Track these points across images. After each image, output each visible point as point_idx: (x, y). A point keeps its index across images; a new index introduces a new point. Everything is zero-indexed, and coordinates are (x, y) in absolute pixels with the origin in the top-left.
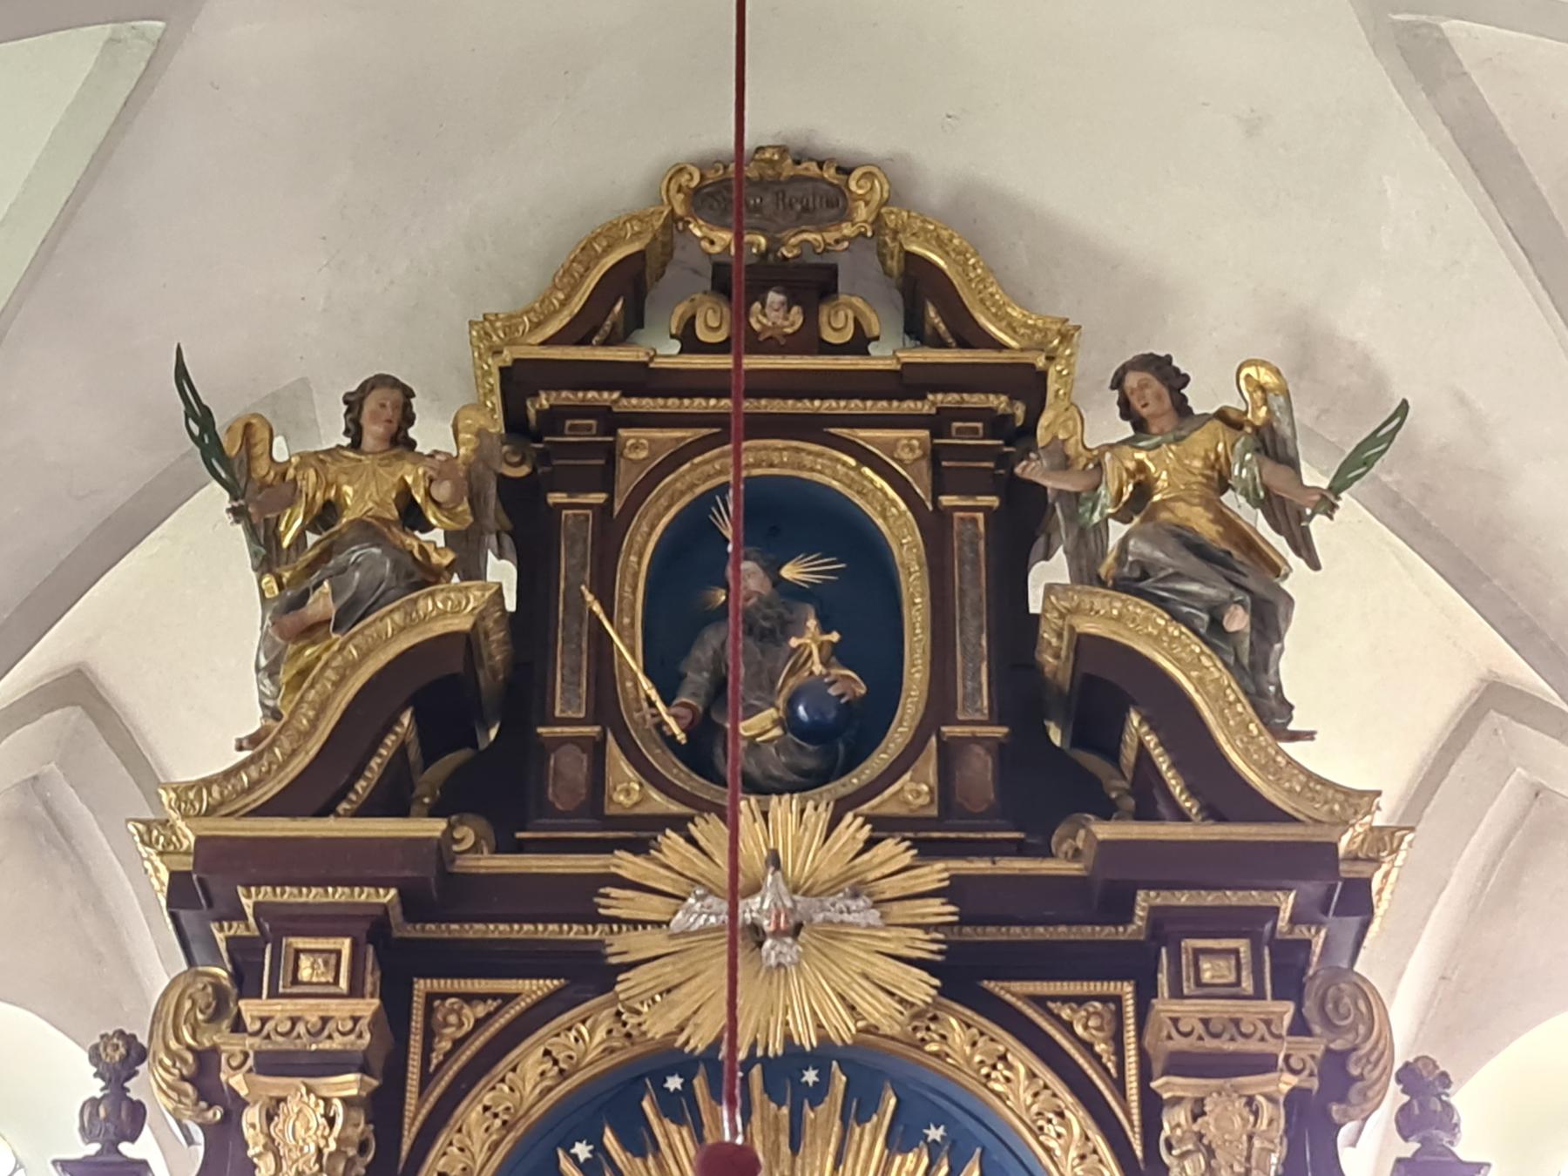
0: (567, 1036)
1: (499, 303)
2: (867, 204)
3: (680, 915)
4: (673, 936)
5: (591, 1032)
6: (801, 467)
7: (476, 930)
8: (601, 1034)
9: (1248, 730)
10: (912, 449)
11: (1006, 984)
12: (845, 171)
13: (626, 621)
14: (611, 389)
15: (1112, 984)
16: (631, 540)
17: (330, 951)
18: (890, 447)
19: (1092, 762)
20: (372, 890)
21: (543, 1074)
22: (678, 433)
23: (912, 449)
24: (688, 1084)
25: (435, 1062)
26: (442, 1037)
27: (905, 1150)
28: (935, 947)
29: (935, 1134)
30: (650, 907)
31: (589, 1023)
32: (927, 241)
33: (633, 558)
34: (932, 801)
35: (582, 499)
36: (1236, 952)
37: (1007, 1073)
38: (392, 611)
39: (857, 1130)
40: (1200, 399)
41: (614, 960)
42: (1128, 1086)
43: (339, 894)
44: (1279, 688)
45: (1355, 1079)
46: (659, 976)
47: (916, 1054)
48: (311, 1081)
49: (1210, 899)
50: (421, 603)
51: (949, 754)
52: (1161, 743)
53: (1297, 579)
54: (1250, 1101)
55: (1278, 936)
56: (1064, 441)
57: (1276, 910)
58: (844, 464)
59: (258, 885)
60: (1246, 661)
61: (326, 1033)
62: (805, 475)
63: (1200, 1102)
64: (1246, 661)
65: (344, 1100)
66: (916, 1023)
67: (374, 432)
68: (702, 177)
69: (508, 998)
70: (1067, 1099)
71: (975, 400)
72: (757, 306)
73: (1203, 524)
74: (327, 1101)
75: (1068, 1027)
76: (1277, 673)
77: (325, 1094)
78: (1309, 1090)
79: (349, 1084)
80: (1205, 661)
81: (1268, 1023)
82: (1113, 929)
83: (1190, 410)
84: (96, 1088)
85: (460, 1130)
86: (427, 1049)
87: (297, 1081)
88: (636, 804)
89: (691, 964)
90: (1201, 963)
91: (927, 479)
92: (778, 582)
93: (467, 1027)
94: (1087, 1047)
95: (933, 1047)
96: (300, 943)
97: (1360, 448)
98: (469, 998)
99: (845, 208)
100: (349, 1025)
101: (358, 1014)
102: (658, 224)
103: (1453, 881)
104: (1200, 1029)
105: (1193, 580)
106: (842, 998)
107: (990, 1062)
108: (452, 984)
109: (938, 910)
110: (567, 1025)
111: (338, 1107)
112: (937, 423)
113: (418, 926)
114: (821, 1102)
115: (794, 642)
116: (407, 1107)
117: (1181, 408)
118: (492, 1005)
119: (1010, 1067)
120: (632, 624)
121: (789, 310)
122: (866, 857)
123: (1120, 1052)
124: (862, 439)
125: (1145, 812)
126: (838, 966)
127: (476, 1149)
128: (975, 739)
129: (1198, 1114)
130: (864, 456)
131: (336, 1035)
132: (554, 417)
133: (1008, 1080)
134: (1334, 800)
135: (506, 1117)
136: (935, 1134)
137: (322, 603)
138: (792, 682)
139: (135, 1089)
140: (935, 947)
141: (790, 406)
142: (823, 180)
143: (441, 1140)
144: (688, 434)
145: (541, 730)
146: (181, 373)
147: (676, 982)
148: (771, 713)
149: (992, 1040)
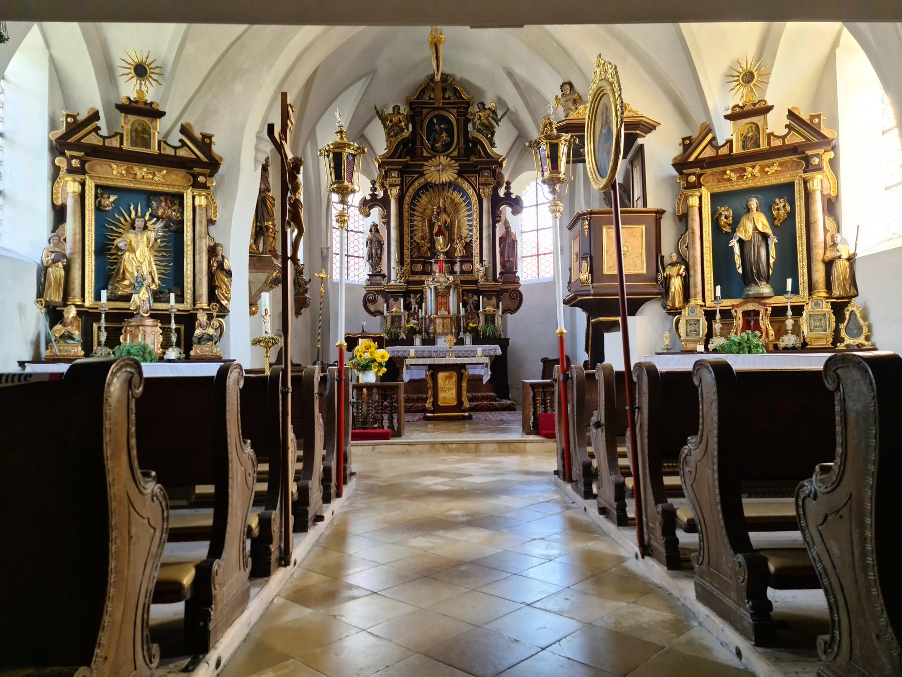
19: (474, 149)
30: (428, 168)
40: (487, 107)
53: (497, 129)
67: (396, 112)
71: (462, 105)
73: (485, 121)
79: (398, 187)
109: (457, 168)
112: (458, 108)
117: (485, 108)
125: (480, 158)
130: (450, 112)
137: (392, 134)
139: (375, 186)
146: (375, 107)
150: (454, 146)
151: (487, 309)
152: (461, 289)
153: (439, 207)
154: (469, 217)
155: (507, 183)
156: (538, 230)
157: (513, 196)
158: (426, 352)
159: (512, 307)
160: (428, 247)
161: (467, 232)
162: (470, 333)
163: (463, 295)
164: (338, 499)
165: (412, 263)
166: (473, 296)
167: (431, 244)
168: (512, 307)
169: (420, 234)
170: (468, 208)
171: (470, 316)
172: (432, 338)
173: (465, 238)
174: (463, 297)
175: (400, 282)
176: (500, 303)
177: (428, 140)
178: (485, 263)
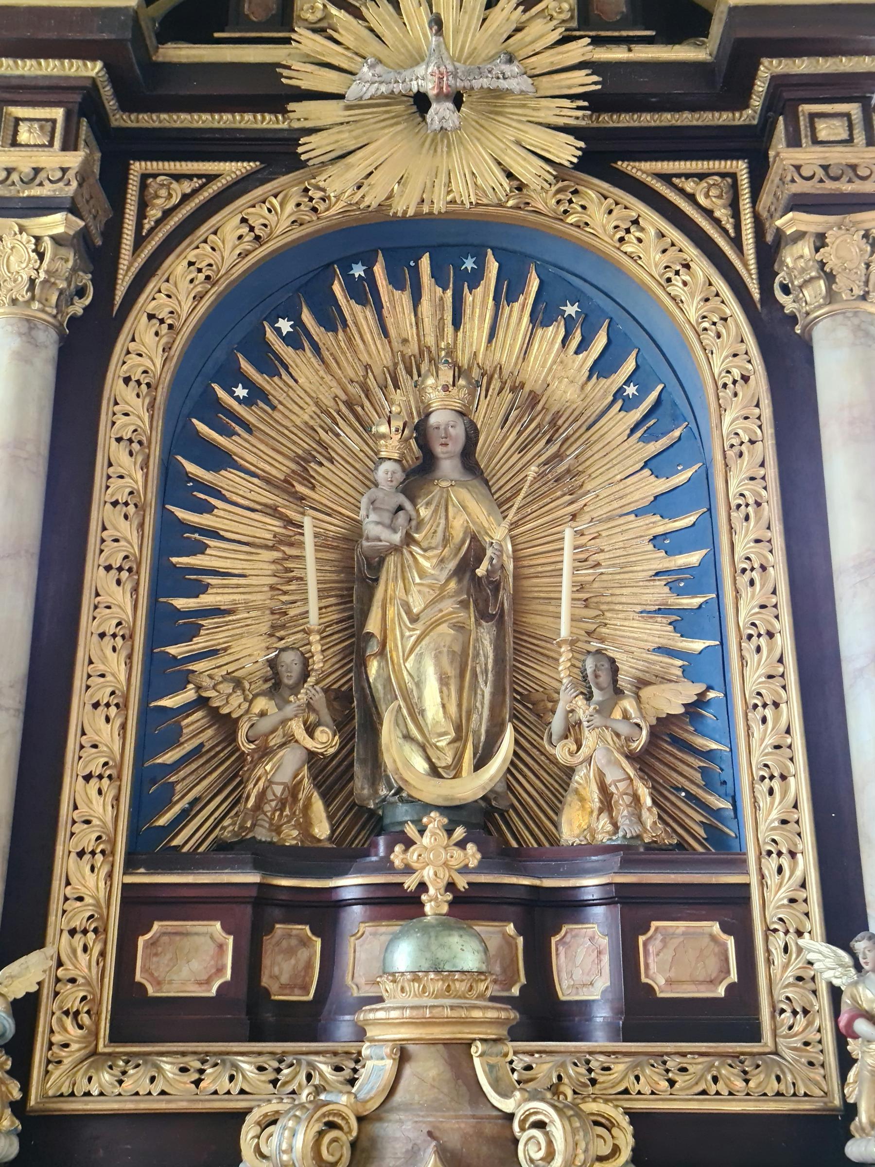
0: (261, 207)
3: (354, 86)
4: (348, 108)
5: (282, 204)
11: (637, 164)
15: (729, 162)
17: (47, 120)
20: (80, 62)
21: (240, 237)
24: (369, 272)
25: (147, 227)
26: (153, 206)
27: (546, 324)
28: (580, 113)
29: (571, 310)
31: (280, 197)
34: (572, 17)
36: (848, 115)
37: (638, 234)
39: (507, 310)
42: (745, 243)
46: (337, 141)
47: (558, 225)
48: (23, 222)
61: (37, 181)
65: (53, 238)
66: (559, 196)
69: (211, 178)
70: (692, 252)
74: (38, 239)
75: (691, 198)
77: (37, 232)
82: (730, 115)
85: (167, 281)
86: (141, 215)
88: (320, 20)
89: (365, 133)
90: (817, 125)
93: (175, 200)
94: (708, 213)
95: (571, 219)
98: (178, 177)
100: (59, 174)
101: (65, 166)
104: (820, 173)
107: (624, 226)
108: (163, 165)
110: (261, 198)
111: (47, 245)
113: (133, 117)
114: (476, 287)
116: (121, 261)
118: (196, 183)
119: (642, 230)
122: (519, 36)
123: (736, 215)
126: (494, 135)
129: (820, 241)
131: (46, 183)
133: (640, 240)
135: (209, 273)
136: (571, 310)
143: (151, 286)
147: (353, 148)
149: (626, 208)
167: (341, 725)
170: (654, 448)
173: (641, 683)
174: (481, 1040)
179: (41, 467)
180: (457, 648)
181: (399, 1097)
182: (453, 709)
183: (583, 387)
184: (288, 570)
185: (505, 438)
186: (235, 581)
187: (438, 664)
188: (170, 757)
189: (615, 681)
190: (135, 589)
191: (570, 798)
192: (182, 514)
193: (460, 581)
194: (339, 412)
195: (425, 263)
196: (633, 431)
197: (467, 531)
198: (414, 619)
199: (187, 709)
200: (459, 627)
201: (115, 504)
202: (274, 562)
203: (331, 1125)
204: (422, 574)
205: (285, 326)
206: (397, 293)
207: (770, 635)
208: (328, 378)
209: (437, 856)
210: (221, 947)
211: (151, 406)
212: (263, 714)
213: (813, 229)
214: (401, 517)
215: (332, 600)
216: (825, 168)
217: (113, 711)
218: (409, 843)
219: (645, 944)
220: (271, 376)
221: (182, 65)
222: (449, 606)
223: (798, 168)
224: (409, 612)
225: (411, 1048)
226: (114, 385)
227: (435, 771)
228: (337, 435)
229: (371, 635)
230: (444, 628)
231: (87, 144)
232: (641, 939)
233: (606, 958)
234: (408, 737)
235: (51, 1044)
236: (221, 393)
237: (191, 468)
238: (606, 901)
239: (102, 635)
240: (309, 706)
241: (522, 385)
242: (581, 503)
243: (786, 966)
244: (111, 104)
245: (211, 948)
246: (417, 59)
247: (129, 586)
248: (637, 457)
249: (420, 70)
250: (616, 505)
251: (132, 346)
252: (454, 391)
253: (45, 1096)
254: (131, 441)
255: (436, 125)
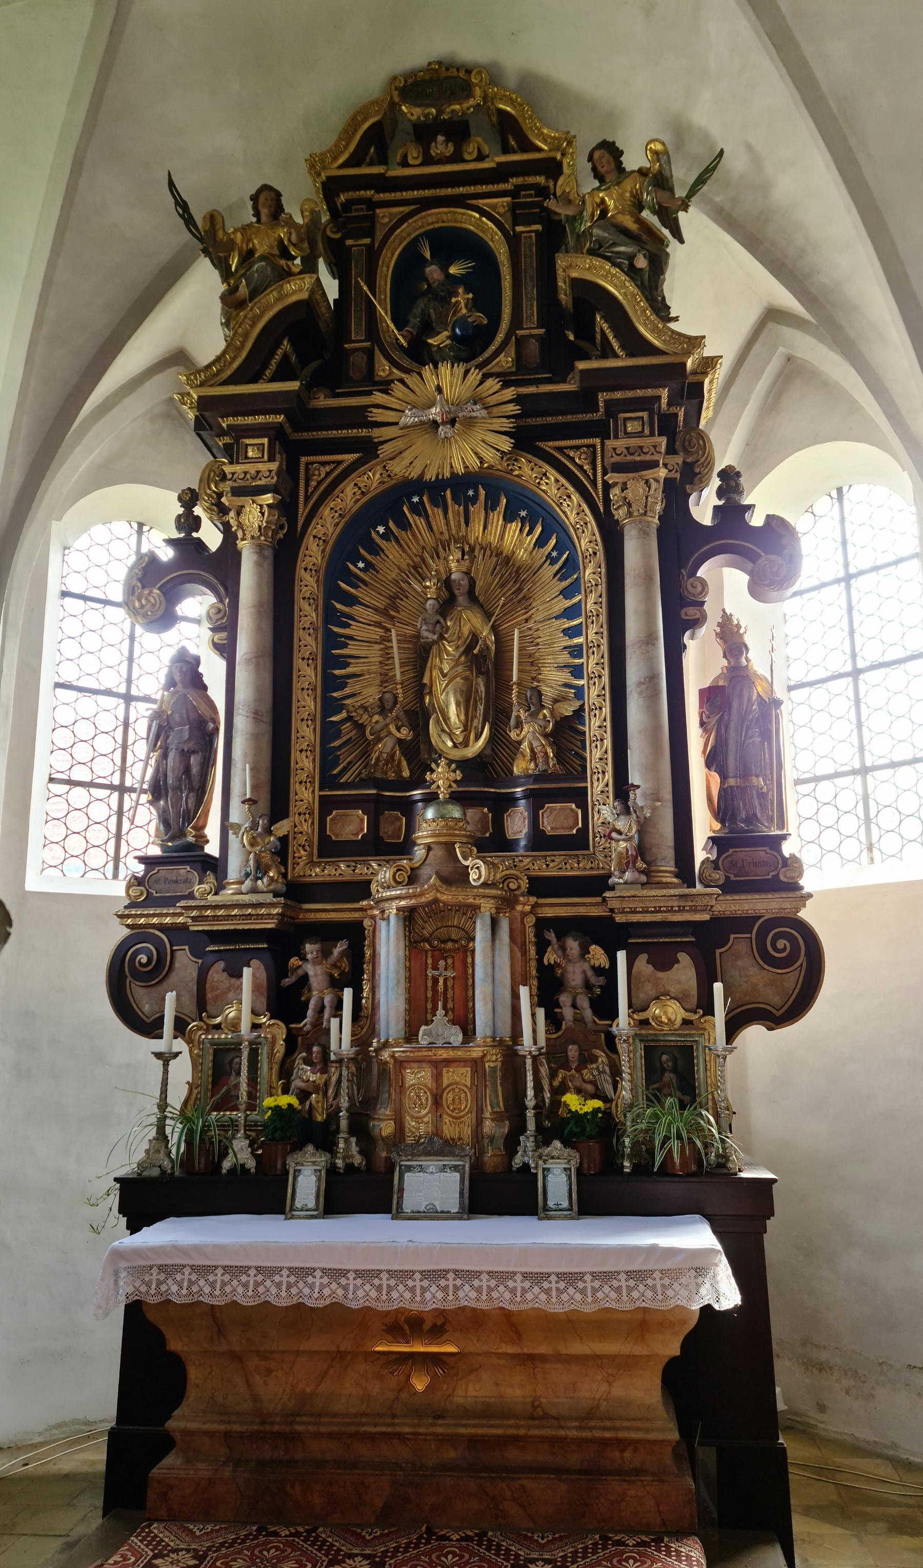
1: (319, 148)
2: (480, 88)
4: (401, 429)
6: (456, 222)
7: (324, 434)
8: (378, 476)
9: (646, 314)
10: (504, 207)
12: (468, 72)
13: (383, 297)
14: (370, 189)
16: (383, 261)
17: (260, 444)
18: (493, 207)
22: (401, 209)
23: (504, 207)
24: (421, 499)
26: (313, 480)
29: (523, 513)
32: (506, 102)
33: (385, 269)
35: (360, 242)
36: (642, 418)
38: (272, 291)
41: (376, 440)
43: (260, 419)
44: (664, 298)
45: (697, 474)
47: (509, 476)
48: (254, 498)
49: (630, 394)
50: (285, 286)
51: (521, 343)
52: (610, 327)
53: (673, 247)
54: (647, 482)
55: (662, 412)
56: (569, 193)
57: (660, 397)
58: (475, 217)
59: (227, 417)
60: (646, 284)
62: (458, 225)
63: (625, 484)
64: (646, 284)
65: (267, 505)
67: (264, 212)
68: (406, 81)
69: (339, 463)
71: (531, 180)
72: (433, 144)
73: (628, 222)
74: (261, 506)
76: (662, 291)
77: (260, 503)
78: (676, 479)
80: (628, 284)
81: (655, 447)
83: (624, 169)
84: (181, 511)
86: (307, 485)
87: (248, 498)
91: (510, 221)
92: (448, 276)
93: (323, 476)
94: (580, 467)
95: (516, 473)
96: (248, 441)
97: (701, 176)
98: (323, 464)
99: (471, 90)
102: (385, 105)
103: (752, 401)
104: (625, 451)
105: (621, 245)
106: (476, 454)
109: (512, 409)
111: (266, 509)
112: (514, 193)
115: (454, 300)
117: (620, 169)
118: (332, 466)
119: (548, 478)
120: (385, 298)
121: (447, 145)
122: (481, 387)
124: (484, 205)
127: (329, 526)
128: (531, 336)
129: (624, 488)
132: (349, 204)
133: (547, 484)
134: (684, 342)
136: (523, 513)
138: (455, 318)
140: (511, 425)
141: (449, 191)
142: (459, 77)
144: (406, 209)
145: (346, 346)
146: (171, 184)
148: (446, 333)
150: (500, 337)
151: (655, 1010)
152: (530, 921)
153: (447, 583)
154: (571, 618)
155: (723, 474)
156: (856, 673)
157: (757, 520)
158: (318, 1280)
159: (776, 1000)
160: (400, 741)
161: (565, 676)
162: (566, 1144)
163: (542, 946)
164: (782, 707)
165: (327, 805)
166: (584, 951)
167: (413, 727)
168: (773, 999)
169: (371, 694)
170: (565, 584)
171: (573, 1051)
172: (380, 1166)
173: (556, 701)
174: (541, 952)
175: (254, 890)
176: (718, 987)
177: (400, 322)
178: (638, 798)
179: (271, 615)
180: (464, 689)
181: (427, 862)
182: (463, 717)
183: (531, 553)
184: (388, 654)
185: (494, 581)
186: (363, 660)
187: (455, 696)
188: (336, 743)
189: (541, 701)
190: (316, 668)
191: (519, 756)
192: (336, 629)
193: (467, 656)
194: (410, 572)
195: (448, 493)
196: (555, 575)
197: (471, 632)
198: (444, 675)
199: (343, 721)
200: (466, 679)
201: (304, 629)
202: (381, 650)
203: (398, 870)
204: (448, 654)
205: (381, 529)
206: (436, 509)
207: (600, 677)
208: (404, 554)
209: (444, 775)
210: (362, 820)
211: (317, 581)
212: (377, 722)
213: (621, 480)
214: (438, 627)
215: (410, 668)
216: (628, 449)
217: (310, 722)
218: (432, 771)
219: (543, 814)
220: (376, 556)
221: (321, 409)
222: (460, 669)
223: (614, 449)
224: (442, 672)
225: (432, 846)
226: (300, 573)
227: (455, 746)
228: (410, 584)
229: (425, 684)
230: (458, 679)
231: (279, 453)
232: (541, 812)
233: (527, 821)
234: (443, 730)
235: (294, 857)
236: (351, 567)
237: (338, 606)
238: (525, 797)
239: (303, 689)
240: (397, 717)
241: (502, 553)
242: (530, 613)
243: (598, 819)
244: (289, 430)
245: (358, 821)
246: (432, 404)
247: (313, 667)
248: (556, 589)
249: (433, 410)
250: (546, 614)
251: (307, 552)
252: (462, 562)
253: (293, 876)
254: (309, 598)
255: (443, 436)
